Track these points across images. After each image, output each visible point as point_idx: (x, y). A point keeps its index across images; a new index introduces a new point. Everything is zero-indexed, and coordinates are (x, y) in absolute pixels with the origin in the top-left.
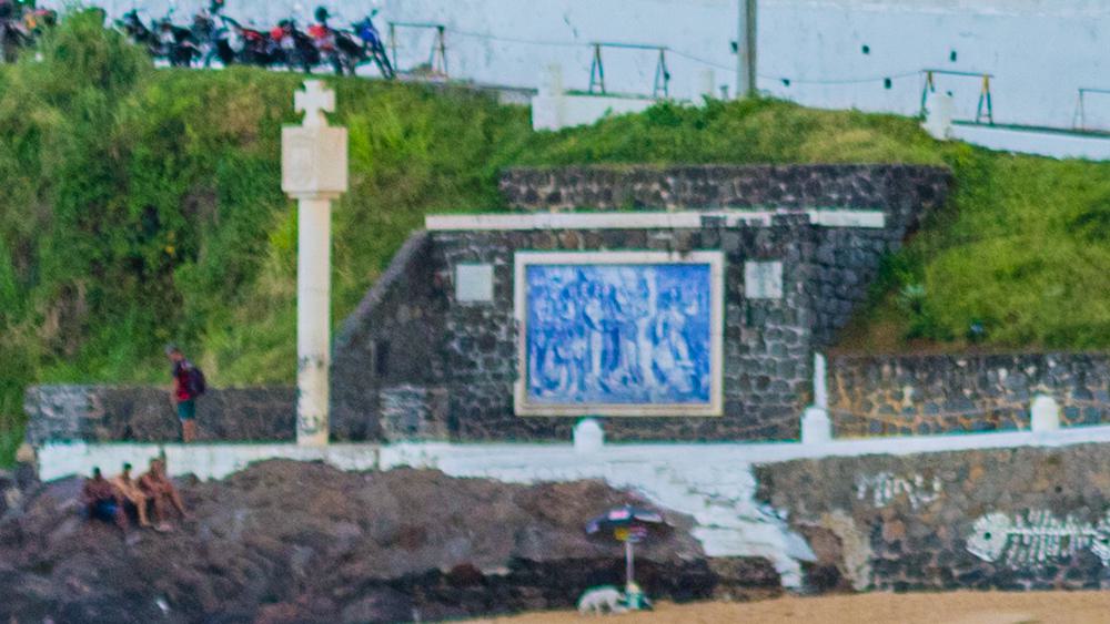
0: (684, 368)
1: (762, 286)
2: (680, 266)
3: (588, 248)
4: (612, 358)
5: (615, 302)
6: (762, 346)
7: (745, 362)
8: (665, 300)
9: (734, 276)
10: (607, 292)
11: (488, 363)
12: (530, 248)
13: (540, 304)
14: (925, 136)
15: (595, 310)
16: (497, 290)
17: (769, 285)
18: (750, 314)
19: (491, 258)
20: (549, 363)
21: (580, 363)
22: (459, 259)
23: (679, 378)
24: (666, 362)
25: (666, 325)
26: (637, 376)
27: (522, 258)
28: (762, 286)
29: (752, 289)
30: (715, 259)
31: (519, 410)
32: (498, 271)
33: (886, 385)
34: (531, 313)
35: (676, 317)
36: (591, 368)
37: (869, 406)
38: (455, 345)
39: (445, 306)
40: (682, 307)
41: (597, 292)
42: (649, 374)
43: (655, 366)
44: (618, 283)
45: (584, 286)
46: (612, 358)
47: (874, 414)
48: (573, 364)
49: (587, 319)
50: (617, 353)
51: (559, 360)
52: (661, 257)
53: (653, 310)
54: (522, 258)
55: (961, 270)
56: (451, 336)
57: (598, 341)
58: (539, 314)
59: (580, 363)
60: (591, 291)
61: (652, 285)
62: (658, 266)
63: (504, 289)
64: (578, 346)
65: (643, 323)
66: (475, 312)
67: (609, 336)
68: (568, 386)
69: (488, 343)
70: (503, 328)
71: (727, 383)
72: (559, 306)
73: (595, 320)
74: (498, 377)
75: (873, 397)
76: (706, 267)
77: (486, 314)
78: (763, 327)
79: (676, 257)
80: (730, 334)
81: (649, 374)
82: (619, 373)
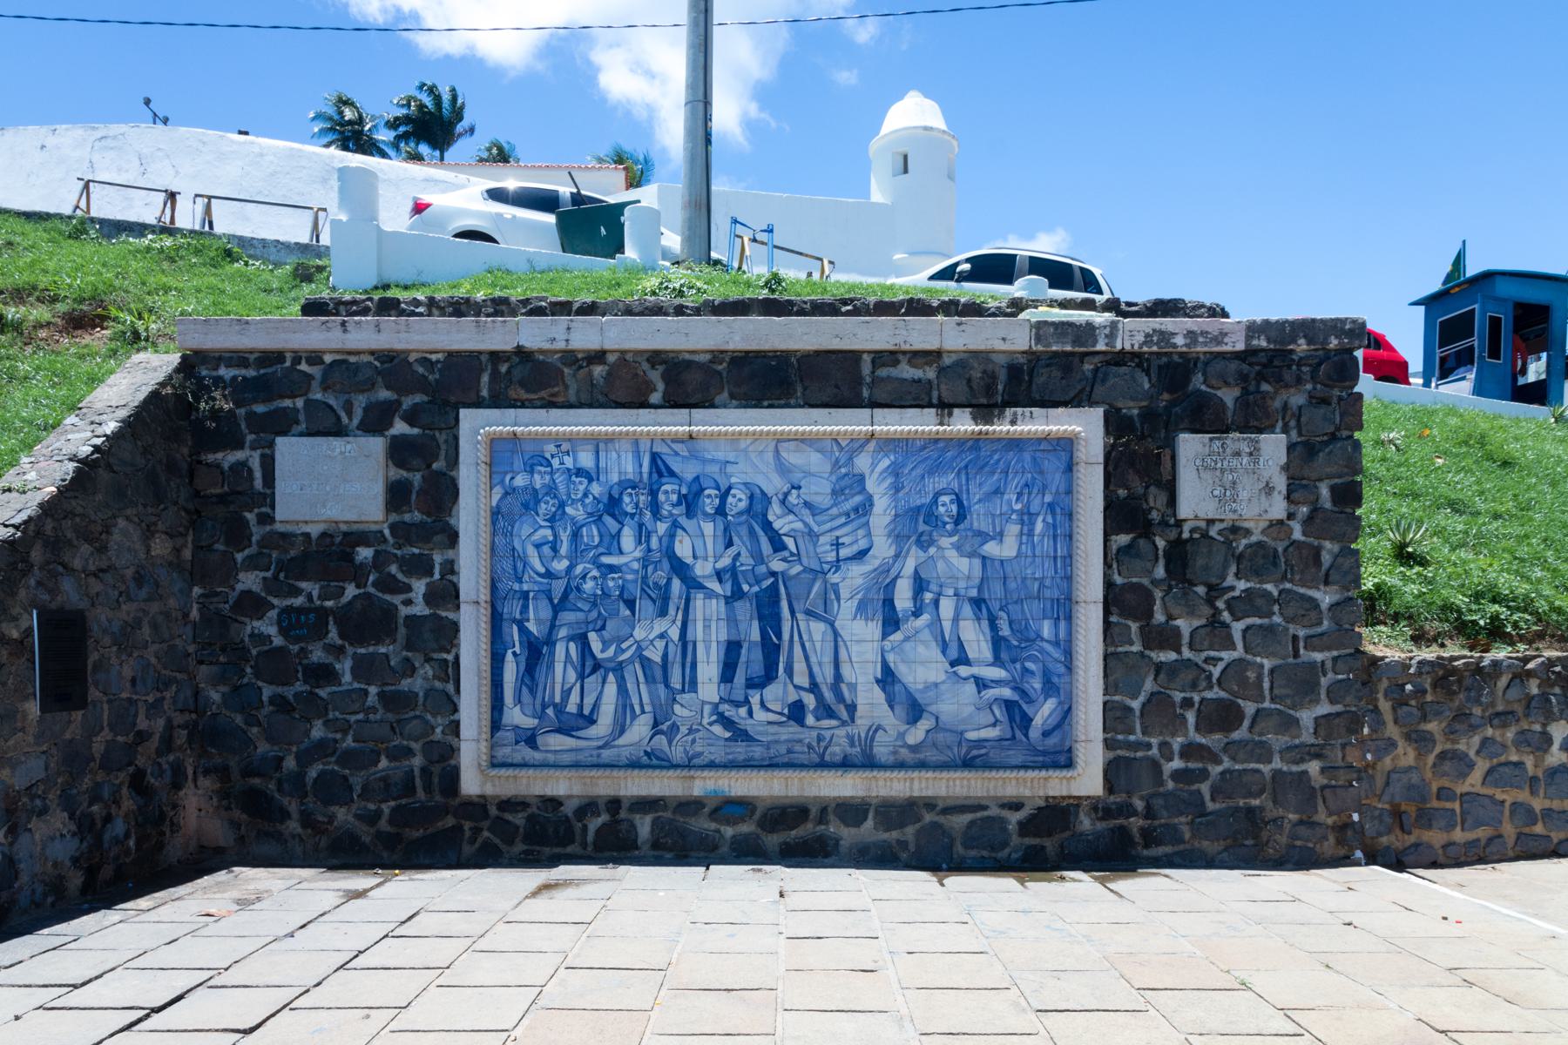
0: (981, 684)
1: (1229, 492)
2: (976, 442)
3: (674, 401)
4: (759, 661)
5: (767, 526)
6: (1216, 631)
7: (1159, 667)
8: (918, 525)
9: (1138, 470)
10: (738, 501)
11: (364, 669)
12: (498, 401)
13: (530, 533)
14: (180, 230)
15: (700, 545)
16: (396, 495)
17: (1247, 489)
18: (1179, 555)
19: (375, 422)
20: (561, 670)
21: (657, 673)
22: (282, 424)
23: (963, 708)
24: (923, 667)
25: (920, 585)
26: (834, 702)
27: (478, 427)
28: (1229, 492)
29: (1195, 499)
30: (1084, 427)
31: (471, 783)
32: (399, 452)
33: (1502, 718)
34: (503, 555)
35: (954, 563)
36: (692, 684)
37: (1464, 764)
38: (267, 626)
39: (237, 534)
40: (974, 541)
41: (709, 504)
42: (870, 701)
43: (887, 678)
44: (773, 484)
45: (669, 492)
46: (759, 661)
47: (1474, 781)
48: (634, 674)
49: (680, 568)
50: (771, 650)
51: (589, 665)
52: (918, 423)
53: (883, 549)
54: (478, 427)
55: (1483, 437)
56: (253, 605)
57: (711, 624)
58: (532, 552)
59: (657, 673)
60: (690, 503)
61: (877, 488)
62: (890, 444)
63: (424, 494)
64: (652, 632)
65: (853, 579)
66: (333, 552)
67: (744, 609)
68: (620, 728)
69: (369, 622)
70: (419, 586)
71: (1114, 716)
72: (591, 534)
73: (702, 569)
74: (393, 701)
75: (1469, 745)
76: (1065, 446)
77: (365, 553)
78: (1215, 590)
79: (963, 424)
80: (392, 364)
81: (870, 701)
82: (777, 694)
